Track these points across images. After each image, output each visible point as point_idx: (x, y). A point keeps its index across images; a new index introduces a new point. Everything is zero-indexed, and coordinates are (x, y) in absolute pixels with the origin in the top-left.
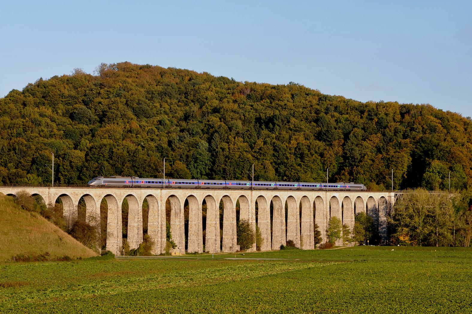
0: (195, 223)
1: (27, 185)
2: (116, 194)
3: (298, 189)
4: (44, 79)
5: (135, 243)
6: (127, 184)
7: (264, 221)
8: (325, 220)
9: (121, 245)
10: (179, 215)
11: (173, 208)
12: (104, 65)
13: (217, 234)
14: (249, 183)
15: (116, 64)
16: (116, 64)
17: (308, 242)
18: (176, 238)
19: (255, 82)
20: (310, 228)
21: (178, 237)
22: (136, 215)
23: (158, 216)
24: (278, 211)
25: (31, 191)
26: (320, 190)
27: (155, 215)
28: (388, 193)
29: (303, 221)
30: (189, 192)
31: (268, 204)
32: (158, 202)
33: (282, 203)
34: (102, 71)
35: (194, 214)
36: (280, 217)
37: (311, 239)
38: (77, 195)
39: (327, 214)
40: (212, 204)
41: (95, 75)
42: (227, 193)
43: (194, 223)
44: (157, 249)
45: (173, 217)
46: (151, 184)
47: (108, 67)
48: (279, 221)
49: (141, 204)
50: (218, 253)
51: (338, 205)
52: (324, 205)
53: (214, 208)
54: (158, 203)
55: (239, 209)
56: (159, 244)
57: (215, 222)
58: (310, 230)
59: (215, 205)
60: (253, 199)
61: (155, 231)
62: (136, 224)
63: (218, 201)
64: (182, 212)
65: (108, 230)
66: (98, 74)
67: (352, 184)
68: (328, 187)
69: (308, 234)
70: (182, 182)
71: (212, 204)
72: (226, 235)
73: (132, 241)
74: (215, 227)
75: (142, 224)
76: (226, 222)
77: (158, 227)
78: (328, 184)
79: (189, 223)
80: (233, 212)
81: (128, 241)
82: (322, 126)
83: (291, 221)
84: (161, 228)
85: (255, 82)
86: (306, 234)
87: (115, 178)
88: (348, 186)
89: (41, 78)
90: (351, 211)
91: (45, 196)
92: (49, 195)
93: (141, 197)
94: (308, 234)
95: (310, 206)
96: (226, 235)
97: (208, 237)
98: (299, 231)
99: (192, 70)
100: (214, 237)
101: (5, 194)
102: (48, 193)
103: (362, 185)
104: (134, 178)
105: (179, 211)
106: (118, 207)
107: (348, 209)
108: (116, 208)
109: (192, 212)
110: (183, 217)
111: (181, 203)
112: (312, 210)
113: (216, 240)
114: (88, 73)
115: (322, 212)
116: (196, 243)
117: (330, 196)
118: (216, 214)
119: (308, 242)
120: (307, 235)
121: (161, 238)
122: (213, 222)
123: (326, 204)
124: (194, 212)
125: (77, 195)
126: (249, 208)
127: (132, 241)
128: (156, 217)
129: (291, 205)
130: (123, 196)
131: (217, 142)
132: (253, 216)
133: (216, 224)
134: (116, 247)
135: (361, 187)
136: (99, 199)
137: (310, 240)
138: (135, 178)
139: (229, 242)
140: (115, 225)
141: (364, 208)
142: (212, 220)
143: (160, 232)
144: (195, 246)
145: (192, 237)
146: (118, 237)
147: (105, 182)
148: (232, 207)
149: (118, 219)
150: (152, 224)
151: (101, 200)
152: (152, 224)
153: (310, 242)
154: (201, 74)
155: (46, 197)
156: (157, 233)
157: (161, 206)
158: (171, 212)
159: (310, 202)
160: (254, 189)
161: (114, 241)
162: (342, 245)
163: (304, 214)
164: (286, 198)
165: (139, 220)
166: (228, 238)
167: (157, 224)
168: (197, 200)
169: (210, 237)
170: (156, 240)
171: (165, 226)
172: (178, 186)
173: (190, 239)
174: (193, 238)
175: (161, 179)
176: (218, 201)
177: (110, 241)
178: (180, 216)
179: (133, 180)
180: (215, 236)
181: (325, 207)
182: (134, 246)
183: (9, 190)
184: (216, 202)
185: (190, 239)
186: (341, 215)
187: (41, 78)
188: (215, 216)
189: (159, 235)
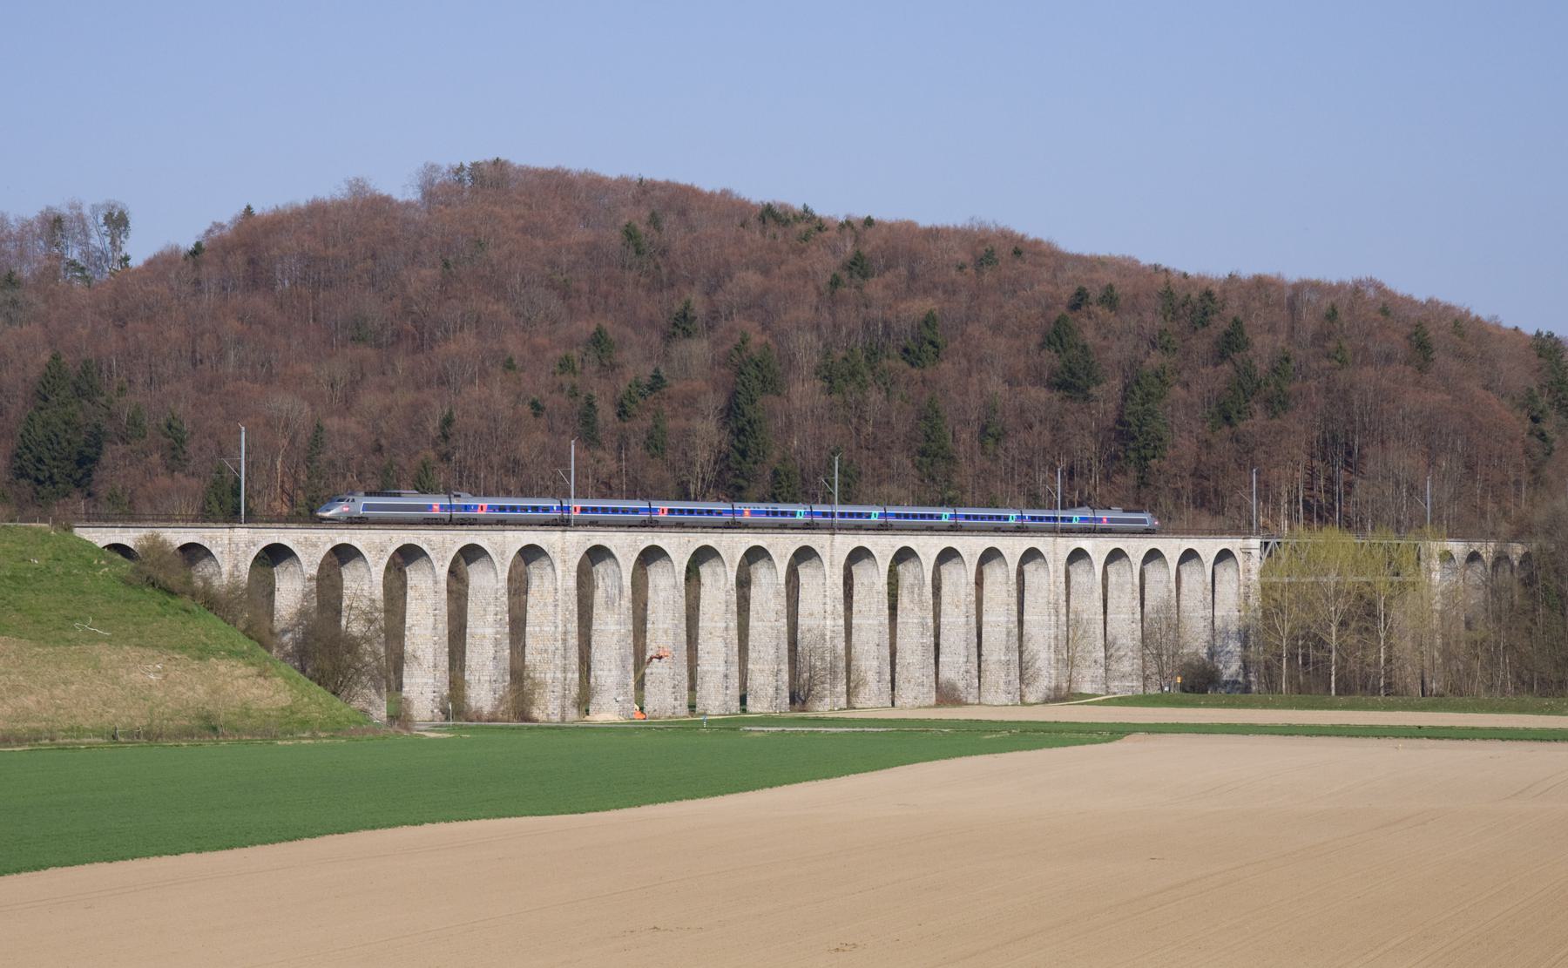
0: (666, 626)
1: (169, 519)
2: (429, 542)
3: (882, 528)
4: (257, 211)
5: (487, 685)
6: (436, 513)
7: (871, 622)
8: (1053, 618)
9: (446, 691)
10: (616, 604)
11: (601, 583)
12: (434, 168)
13: (730, 659)
14: (802, 511)
15: (467, 165)
16: (467, 165)
17: (1001, 683)
18: (610, 670)
19: (869, 217)
20: (1008, 641)
21: (610, 668)
22: (489, 604)
23: (556, 606)
24: (913, 592)
25: (178, 536)
26: (809, 527)
27: (545, 604)
28: (1241, 540)
29: (988, 623)
30: (645, 539)
31: (881, 570)
32: (556, 565)
33: (922, 569)
34: (429, 193)
35: (661, 599)
36: (917, 609)
37: (1012, 674)
38: (315, 545)
39: (1057, 600)
40: (714, 573)
41: (406, 198)
42: (758, 539)
43: (661, 626)
44: (550, 707)
45: (599, 610)
46: (457, 514)
47: (443, 175)
48: (915, 621)
49: (503, 571)
50: (734, 714)
51: (1091, 576)
52: (1049, 575)
53: (723, 582)
54: (554, 570)
55: (451, 584)
56: (559, 689)
57: (725, 625)
58: (1007, 648)
59: (723, 574)
60: (836, 556)
61: (546, 651)
62: (489, 631)
63: (732, 561)
64: (625, 594)
65: (409, 647)
66: (415, 193)
67: (1116, 513)
68: (837, 519)
69: (1003, 658)
70: (997, 516)
71: (714, 573)
72: (756, 662)
73: (479, 680)
74: (725, 639)
75: (507, 630)
76: (756, 624)
77: (556, 640)
78: (838, 509)
79: (649, 626)
80: (778, 593)
81: (466, 678)
82: (1058, 344)
83: (951, 620)
84: (565, 641)
85: (869, 217)
86: (994, 658)
87: (399, 495)
88: (1108, 519)
89: (249, 208)
90: (1129, 590)
91: (220, 549)
92: (233, 545)
93: (503, 553)
94: (1003, 658)
95: (1008, 576)
96: (756, 662)
97: (705, 668)
98: (975, 650)
99: (689, 184)
100: (722, 669)
101: (100, 545)
102: (227, 542)
103: (1146, 516)
104: (455, 496)
105: (617, 592)
106: (436, 582)
107: (1121, 587)
108: (430, 583)
109: (658, 595)
110: (628, 609)
111: (622, 568)
112: (1013, 587)
113: (726, 676)
114: (385, 193)
115: (1044, 593)
116: (669, 683)
117: (1067, 547)
118: (727, 602)
119: (1001, 683)
120: (1000, 661)
121: (565, 670)
122: (718, 625)
123: (1056, 571)
124: (662, 594)
125: (315, 545)
126: (824, 584)
127: (479, 680)
128: (550, 609)
129: (950, 573)
130: (451, 549)
131: (753, 390)
132: (838, 606)
133: (727, 628)
134: (431, 696)
135: (1144, 521)
136: (380, 559)
137: (1008, 675)
138: (459, 496)
139: (767, 682)
140: (429, 633)
141: (1169, 582)
142: (716, 618)
143: (561, 651)
144: (664, 698)
145: (657, 668)
146: (435, 666)
147: (367, 507)
148: (775, 579)
149: (435, 615)
150: (537, 629)
151: (386, 559)
152: (537, 629)
153: (1008, 683)
154: (712, 195)
155: (222, 553)
156: (550, 656)
157: (564, 576)
158: (596, 596)
159: (1007, 565)
160: (840, 529)
161: (425, 680)
162: (1102, 690)
163: (991, 599)
164: (1064, 556)
165: (499, 617)
166: (762, 671)
167: (553, 629)
168: (671, 561)
169: (710, 668)
170: (548, 675)
171: (575, 635)
172: (461, 517)
173: (652, 674)
174: (660, 670)
175: (829, 506)
176: (732, 561)
177: (413, 680)
178: (620, 605)
179: (455, 502)
180: (722, 664)
181: (1052, 581)
182: (483, 693)
183: (115, 532)
184: (727, 565)
185: (652, 674)
186: (1100, 604)
187: (249, 208)
188: (724, 608)
189: (559, 662)
